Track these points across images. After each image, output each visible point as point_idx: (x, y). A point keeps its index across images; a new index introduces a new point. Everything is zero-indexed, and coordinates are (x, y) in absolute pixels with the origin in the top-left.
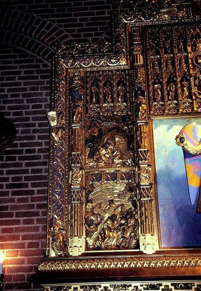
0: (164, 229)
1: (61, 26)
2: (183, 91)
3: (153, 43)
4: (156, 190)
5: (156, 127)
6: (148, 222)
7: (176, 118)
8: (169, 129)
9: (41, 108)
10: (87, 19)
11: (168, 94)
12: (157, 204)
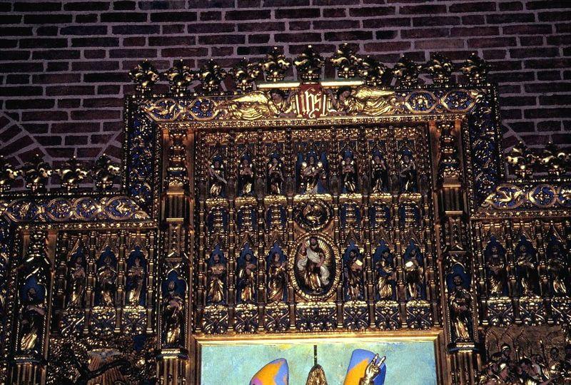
1: (15, 116)
3: (215, 169)
7: (326, 338)
9: (27, 58)
10: (75, 103)
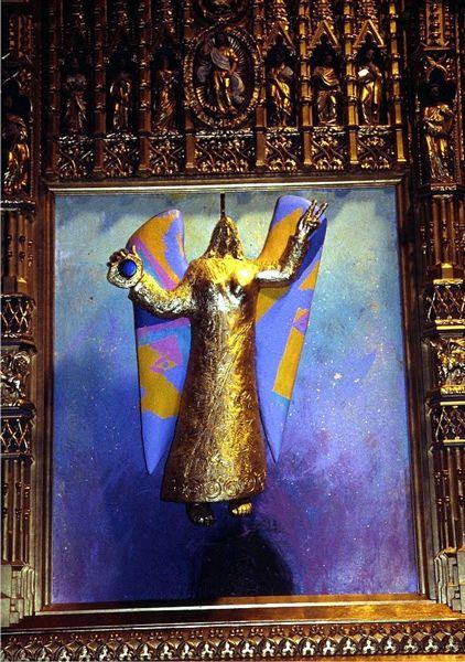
0: (60, 545)
2: (157, 99)
4: (48, 424)
5: (66, 219)
8: (105, 227)
11: (109, 110)
12: (46, 471)
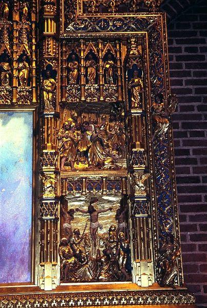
6: (50, 248)
8: (4, 124)
